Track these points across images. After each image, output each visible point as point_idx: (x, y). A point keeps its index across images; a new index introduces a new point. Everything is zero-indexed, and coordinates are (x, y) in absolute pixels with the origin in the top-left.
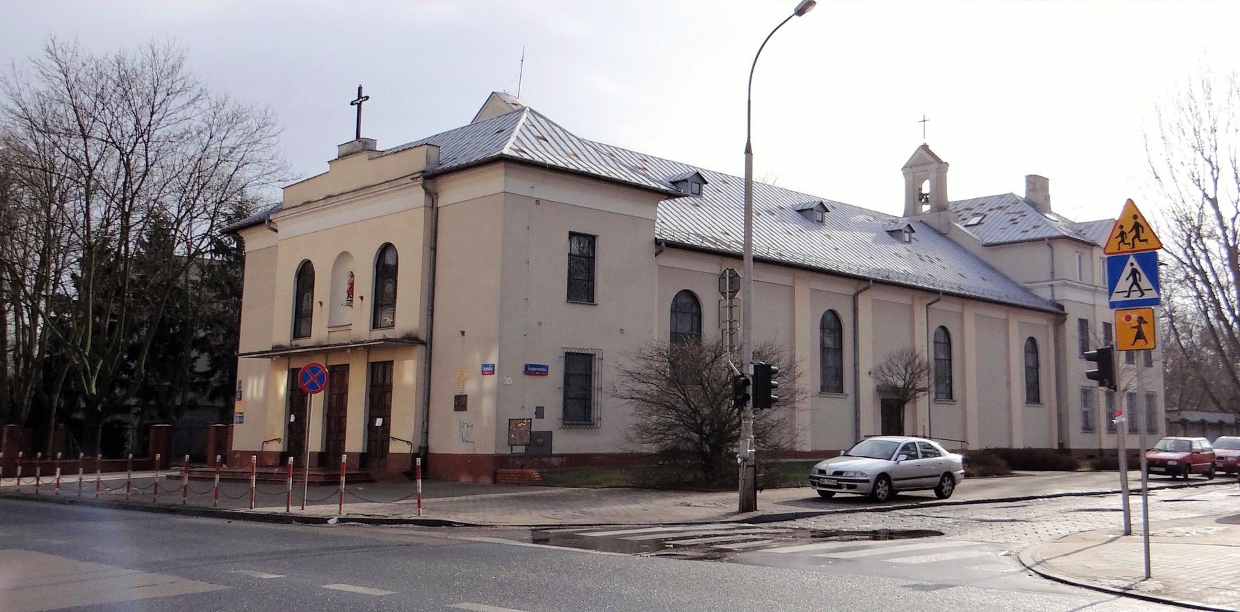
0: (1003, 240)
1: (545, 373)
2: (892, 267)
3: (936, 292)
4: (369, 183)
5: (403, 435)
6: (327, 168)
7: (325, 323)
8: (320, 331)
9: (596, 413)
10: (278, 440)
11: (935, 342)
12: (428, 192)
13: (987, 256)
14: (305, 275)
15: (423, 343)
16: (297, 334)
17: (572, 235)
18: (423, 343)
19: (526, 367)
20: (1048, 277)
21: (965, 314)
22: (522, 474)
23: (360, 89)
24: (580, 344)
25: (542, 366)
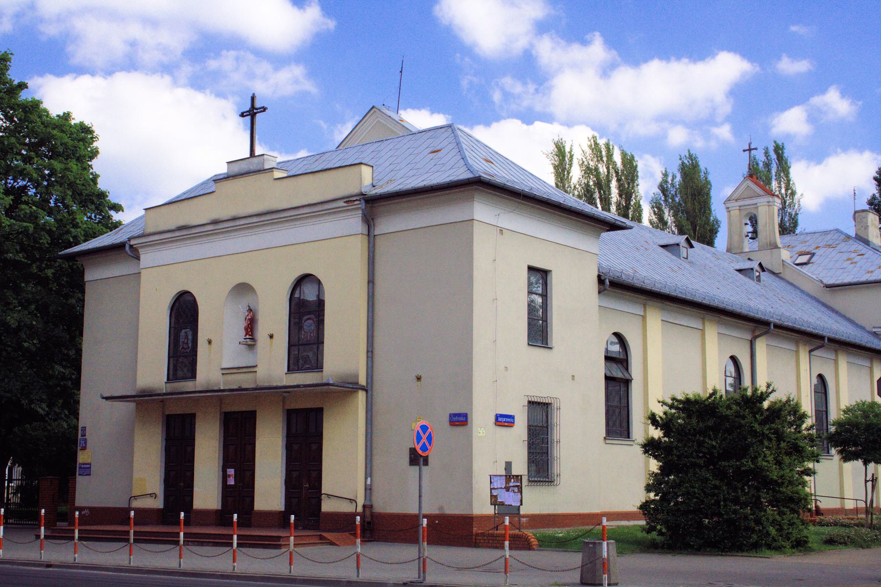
0: (847, 280)
2: (752, 304)
3: (822, 338)
9: (556, 470)
10: (153, 495)
11: (815, 392)
13: (827, 298)
14: (184, 311)
15: (363, 389)
16: (173, 375)
17: (531, 269)
18: (363, 389)
19: (451, 415)
21: (840, 362)
23: (253, 99)
24: (541, 394)
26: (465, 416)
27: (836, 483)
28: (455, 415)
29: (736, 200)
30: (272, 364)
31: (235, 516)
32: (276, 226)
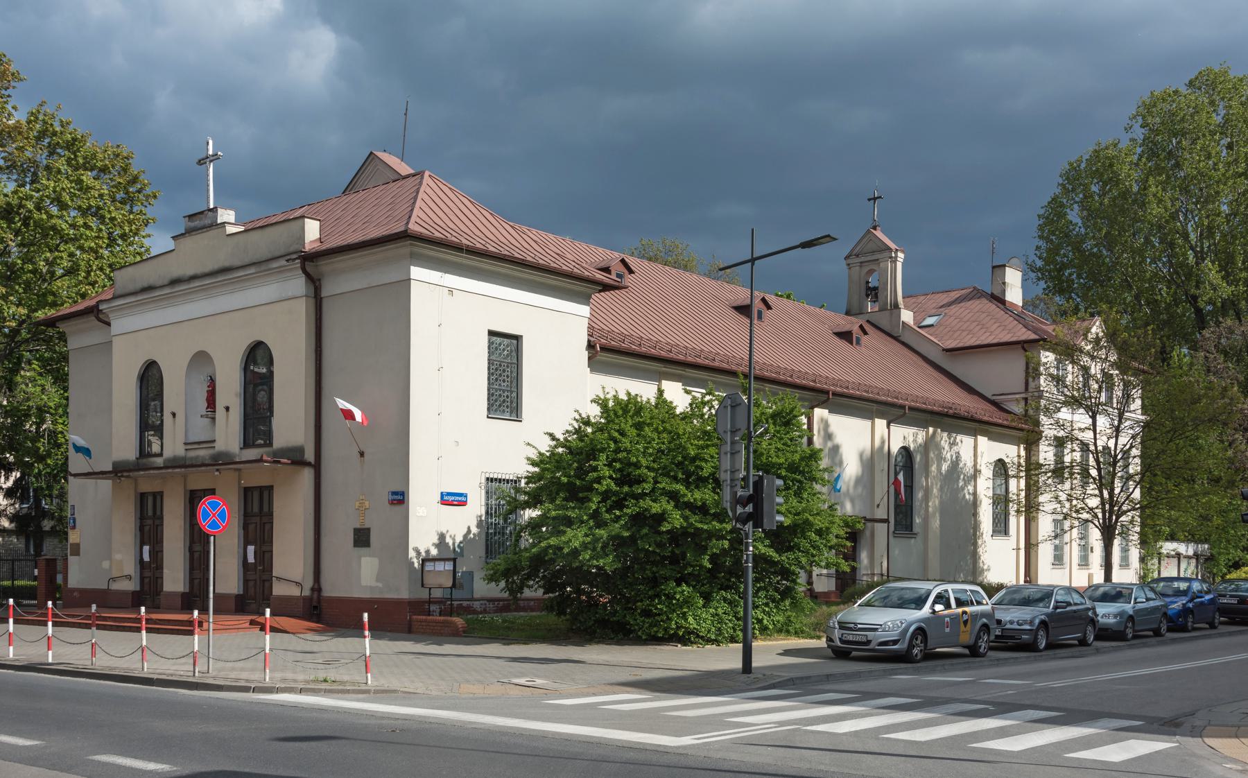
1: (463, 504)
4: (259, 232)
5: (290, 568)
6: (171, 245)
7: (181, 439)
8: (172, 444)
10: (129, 577)
12: (308, 276)
14: (150, 378)
17: (492, 333)
20: (1023, 389)
22: (443, 622)
25: (461, 495)
26: (403, 494)
27: (6, 524)
28: (449, 494)
29: (857, 256)
30: (228, 433)
31: (366, 615)
32: (203, 289)
